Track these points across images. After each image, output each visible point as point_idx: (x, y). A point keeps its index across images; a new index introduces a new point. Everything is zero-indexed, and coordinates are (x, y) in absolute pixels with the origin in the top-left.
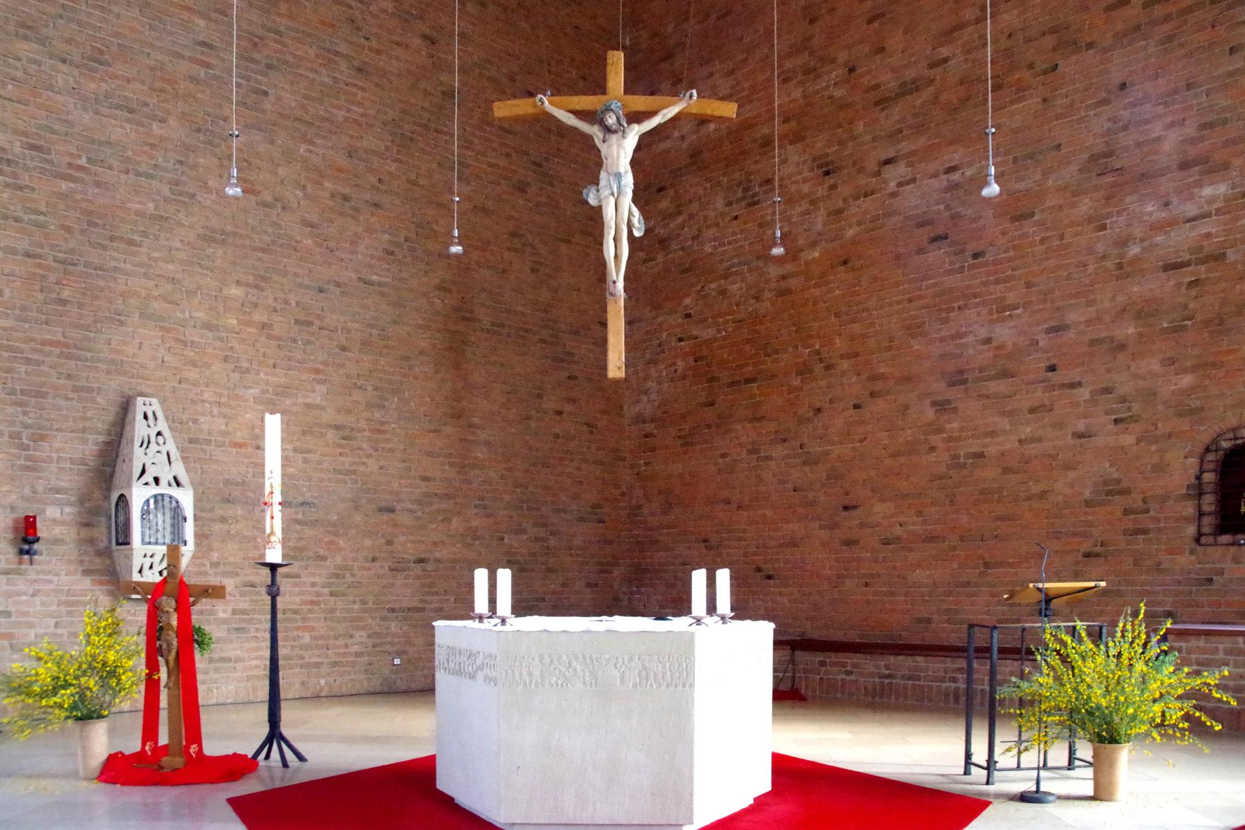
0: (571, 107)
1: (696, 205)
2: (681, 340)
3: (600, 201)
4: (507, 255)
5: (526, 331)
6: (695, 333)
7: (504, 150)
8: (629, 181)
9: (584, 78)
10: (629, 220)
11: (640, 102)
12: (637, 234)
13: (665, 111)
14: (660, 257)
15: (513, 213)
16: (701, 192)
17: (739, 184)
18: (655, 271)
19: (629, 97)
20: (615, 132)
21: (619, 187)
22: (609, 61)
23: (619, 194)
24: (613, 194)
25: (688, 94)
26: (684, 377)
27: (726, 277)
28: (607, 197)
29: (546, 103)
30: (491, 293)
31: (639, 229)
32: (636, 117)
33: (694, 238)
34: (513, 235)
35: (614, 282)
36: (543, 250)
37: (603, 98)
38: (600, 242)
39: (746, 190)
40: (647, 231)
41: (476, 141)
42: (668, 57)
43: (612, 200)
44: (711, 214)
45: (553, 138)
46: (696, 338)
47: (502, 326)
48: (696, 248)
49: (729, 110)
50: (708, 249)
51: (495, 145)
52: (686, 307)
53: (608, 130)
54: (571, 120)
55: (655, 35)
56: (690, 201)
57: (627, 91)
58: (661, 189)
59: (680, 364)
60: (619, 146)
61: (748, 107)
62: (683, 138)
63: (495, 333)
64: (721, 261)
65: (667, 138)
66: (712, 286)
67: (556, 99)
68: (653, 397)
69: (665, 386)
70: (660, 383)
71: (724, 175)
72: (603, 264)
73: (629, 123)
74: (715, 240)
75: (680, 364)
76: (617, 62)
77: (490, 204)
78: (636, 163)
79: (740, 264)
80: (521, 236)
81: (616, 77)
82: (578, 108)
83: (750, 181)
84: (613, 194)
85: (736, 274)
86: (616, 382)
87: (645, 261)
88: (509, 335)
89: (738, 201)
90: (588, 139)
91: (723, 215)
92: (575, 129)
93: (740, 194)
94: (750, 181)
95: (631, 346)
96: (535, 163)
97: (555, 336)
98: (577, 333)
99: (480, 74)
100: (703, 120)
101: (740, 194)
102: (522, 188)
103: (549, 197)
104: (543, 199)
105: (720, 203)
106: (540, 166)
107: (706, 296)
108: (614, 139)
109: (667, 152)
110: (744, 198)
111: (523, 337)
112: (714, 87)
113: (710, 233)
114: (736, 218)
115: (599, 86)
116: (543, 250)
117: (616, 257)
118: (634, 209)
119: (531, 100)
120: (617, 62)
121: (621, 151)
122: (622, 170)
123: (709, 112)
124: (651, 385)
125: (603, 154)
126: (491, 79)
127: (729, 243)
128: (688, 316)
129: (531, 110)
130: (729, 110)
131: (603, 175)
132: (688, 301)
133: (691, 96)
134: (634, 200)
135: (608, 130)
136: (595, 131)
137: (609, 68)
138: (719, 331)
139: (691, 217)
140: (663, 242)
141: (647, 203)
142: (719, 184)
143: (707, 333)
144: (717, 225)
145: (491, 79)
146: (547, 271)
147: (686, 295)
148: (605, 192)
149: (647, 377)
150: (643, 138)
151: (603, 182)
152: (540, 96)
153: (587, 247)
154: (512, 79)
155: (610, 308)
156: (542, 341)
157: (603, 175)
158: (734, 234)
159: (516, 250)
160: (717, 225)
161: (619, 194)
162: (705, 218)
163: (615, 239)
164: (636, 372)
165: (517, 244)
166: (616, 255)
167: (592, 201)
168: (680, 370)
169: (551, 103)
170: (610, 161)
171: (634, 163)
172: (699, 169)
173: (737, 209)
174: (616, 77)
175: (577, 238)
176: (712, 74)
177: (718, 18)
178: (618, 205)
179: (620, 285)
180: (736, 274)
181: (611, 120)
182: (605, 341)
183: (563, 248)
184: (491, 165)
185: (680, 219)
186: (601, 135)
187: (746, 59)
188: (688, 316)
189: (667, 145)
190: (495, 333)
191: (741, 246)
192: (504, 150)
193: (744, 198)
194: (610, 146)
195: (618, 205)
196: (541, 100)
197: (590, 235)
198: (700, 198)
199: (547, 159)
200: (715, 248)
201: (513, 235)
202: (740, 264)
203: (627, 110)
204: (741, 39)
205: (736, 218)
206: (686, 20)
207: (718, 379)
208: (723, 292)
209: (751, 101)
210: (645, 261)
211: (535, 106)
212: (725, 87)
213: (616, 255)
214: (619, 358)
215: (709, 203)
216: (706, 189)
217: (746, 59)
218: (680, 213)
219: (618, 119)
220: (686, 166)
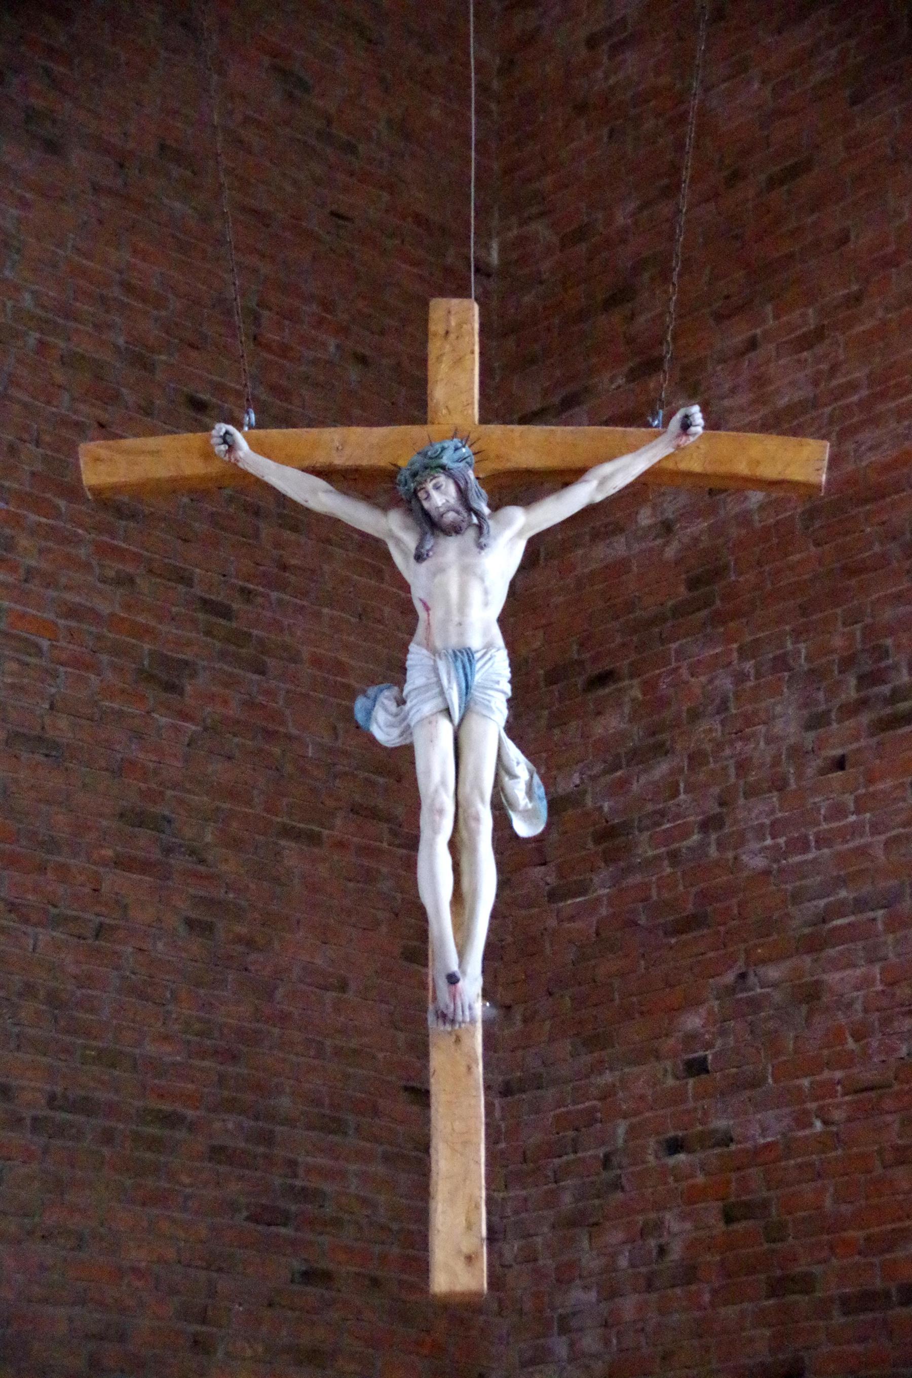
0: (321, 458)
1: (710, 728)
2: (675, 1146)
3: (407, 731)
4: (114, 882)
5: (171, 1120)
6: (720, 1123)
7: (114, 567)
8: (496, 671)
9: (362, 360)
10: (498, 787)
11: (528, 445)
12: (523, 828)
13: (607, 468)
14: (601, 887)
15: (136, 752)
16: (725, 683)
17: (848, 662)
18: (585, 926)
19: (496, 430)
20: (456, 530)
21: (467, 690)
22: (436, 326)
23: (466, 710)
24: (447, 712)
25: (675, 422)
26: (689, 1274)
27: (813, 945)
28: (429, 721)
29: (252, 452)
30: (53, 999)
31: (529, 816)
32: (518, 487)
33: (709, 824)
34: (138, 819)
35: (453, 979)
36: (230, 866)
37: (415, 431)
38: (410, 842)
39: (868, 679)
40: (556, 806)
41: (24, 542)
42: (620, 296)
43: (445, 729)
44: (760, 750)
45: (266, 530)
46: (727, 1140)
47: (86, 1106)
48: (713, 852)
49: (804, 461)
50: (755, 861)
51: (82, 552)
52: (691, 1038)
53: (431, 525)
54: (321, 498)
55: (581, 234)
56: (695, 715)
57: (492, 412)
58: (604, 678)
59: (677, 1227)
60: (467, 570)
61: (867, 436)
62: (667, 528)
63: (60, 1131)
64: (797, 897)
65: (619, 529)
66: (773, 973)
67: (275, 434)
68: (590, 1342)
69: (628, 1305)
70: (611, 1292)
71: (797, 634)
72: (417, 917)
73: (495, 507)
74: (775, 829)
75: (677, 1227)
76: (458, 331)
77: (62, 728)
78: (520, 614)
79: (860, 905)
80: (159, 823)
81: (457, 373)
82: (339, 461)
83: (884, 653)
84: (447, 712)
85: (850, 934)
86: (460, 1311)
87: (554, 896)
88: (108, 1137)
89: (851, 710)
90: (374, 550)
91: (797, 753)
92: (333, 522)
93: (850, 692)
94: (884, 653)
95: (510, 1164)
96: (207, 605)
97: (268, 1139)
98: (335, 1126)
99: (42, 345)
100: (714, 490)
101: (850, 692)
102: (167, 676)
103: (250, 704)
104: (234, 710)
105: (786, 719)
106: (225, 612)
107: (755, 1004)
108: (450, 549)
109: (619, 567)
110: (863, 703)
111: (154, 1144)
112: (760, 381)
113: (756, 812)
114: (840, 764)
115: (405, 397)
116: (230, 866)
117: (458, 898)
118: (514, 753)
119: (194, 439)
120: (458, 331)
121: (472, 588)
122: (475, 642)
123: (742, 468)
124: (581, 1296)
125: (418, 593)
126: (70, 361)
127: (822, 841)
128: (697, 1067)
129: (193, 467)
130: (804, 461)
131: (417, 657)
132: (693, 1021)
133: (686, 425)
134: (515, 729)
135: (431, 525)
136: (393, 528)
137: (434, 347)
138: (802, 1121)
139: (696, 759)
140: (611, 837)
141: (558, 720)
142: (781, 663)
143: (764, 1126)
144: (779, 784)
145: (70, 361)
146: (241, 929)
147: (692, 1002)
148: (422, 707)
149: (566, 1275)
150: (537, 550)
151: (416, 677)
152: (222, 428)
153: (365, 851)
154: (141, 361)
155: (438, 1059)
156: (217, 1153)
157: (417, 656)
158: (838, 811)
159: (145, 867)
160: (779, 784)
161: (466, 710)
162: (743, 766)
163: (454, 846)
164: (530, 1257)
165: (144, 843)
166: (458, 893)
167: (384, 732)
168: (676, 1252)
169: (257, 447)
170: (437, 614)
171: (507, 621)
172: (719, 618)
173: (840, 738)
174: (457, 373)
175: (340, 826)
176: (752, 344)
177: (773, 183)
178: (464, 747)
179: (472, 985)
180: (850, 934)
181: (441, 497)
182: (424, 1147)
183: (292, 855)
184: (73, 612)
185: (662, 769)
186: (410, 540)
187: (857, 298)
188: (697, 1067)
189: (619, 547)
190: (60, 1131)
191: (862, 852)
192: (114, 567)
193: (863, 703)
194: (441, 570)
195: (464, 747)
196: (226, 438)
197: (373, 814)
198: (723, 707)
199: (247, 594)
200: (777, 854)
201: (138, 819)
202: (860, 905)
203: (491, 466)
204: (843, 239)
205: (840, 764)
206: (671, 191)
207: (806, 1283)
208: (810, 994)
209: (875, 421)
210: (554, 896)
211: (208, 454)
212: (790, 384)
213: (458, 893)
214: (470, 1226)
215: (749, 720)
216: (740, 678)
217: (857, 298)
218: (661, 750)
219: (463, 494)
220: (680, 611)
